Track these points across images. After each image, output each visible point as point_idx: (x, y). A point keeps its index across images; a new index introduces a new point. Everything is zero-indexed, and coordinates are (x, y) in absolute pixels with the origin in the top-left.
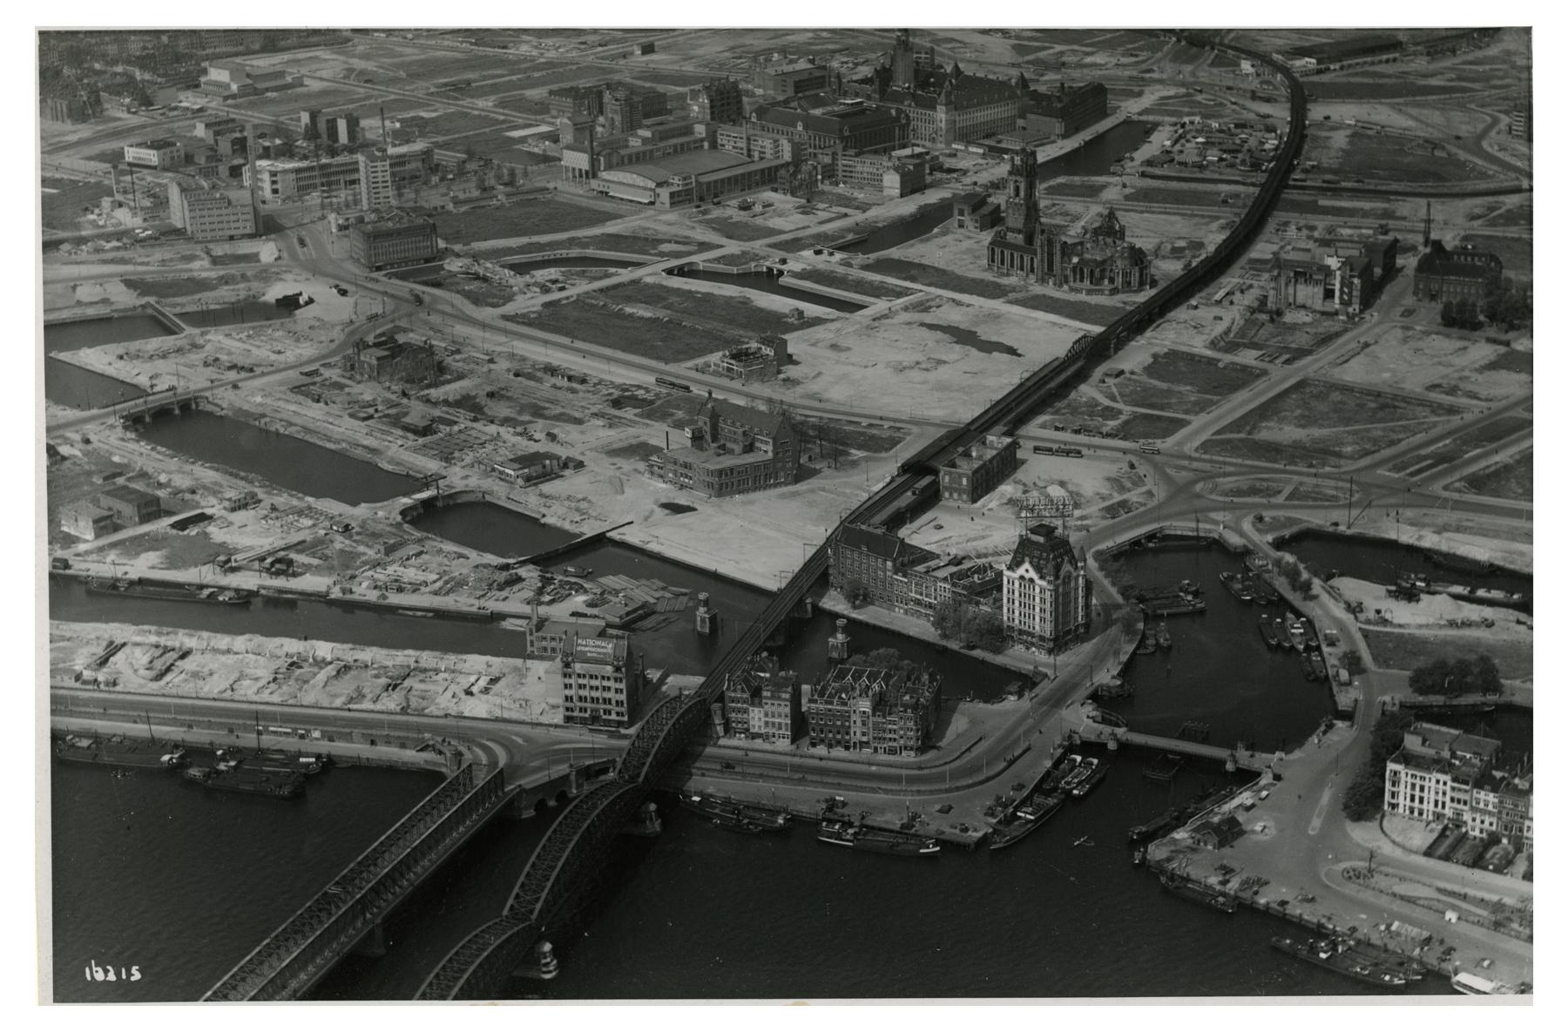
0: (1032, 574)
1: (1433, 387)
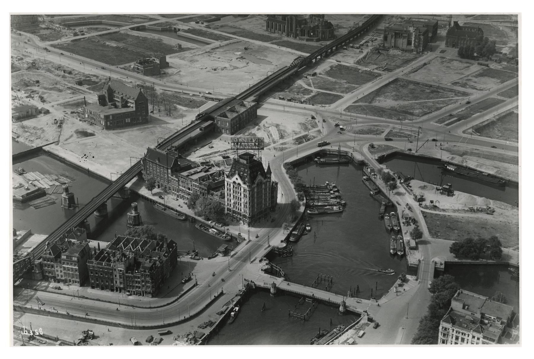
0: (239, 181)
1: (455, 84)
